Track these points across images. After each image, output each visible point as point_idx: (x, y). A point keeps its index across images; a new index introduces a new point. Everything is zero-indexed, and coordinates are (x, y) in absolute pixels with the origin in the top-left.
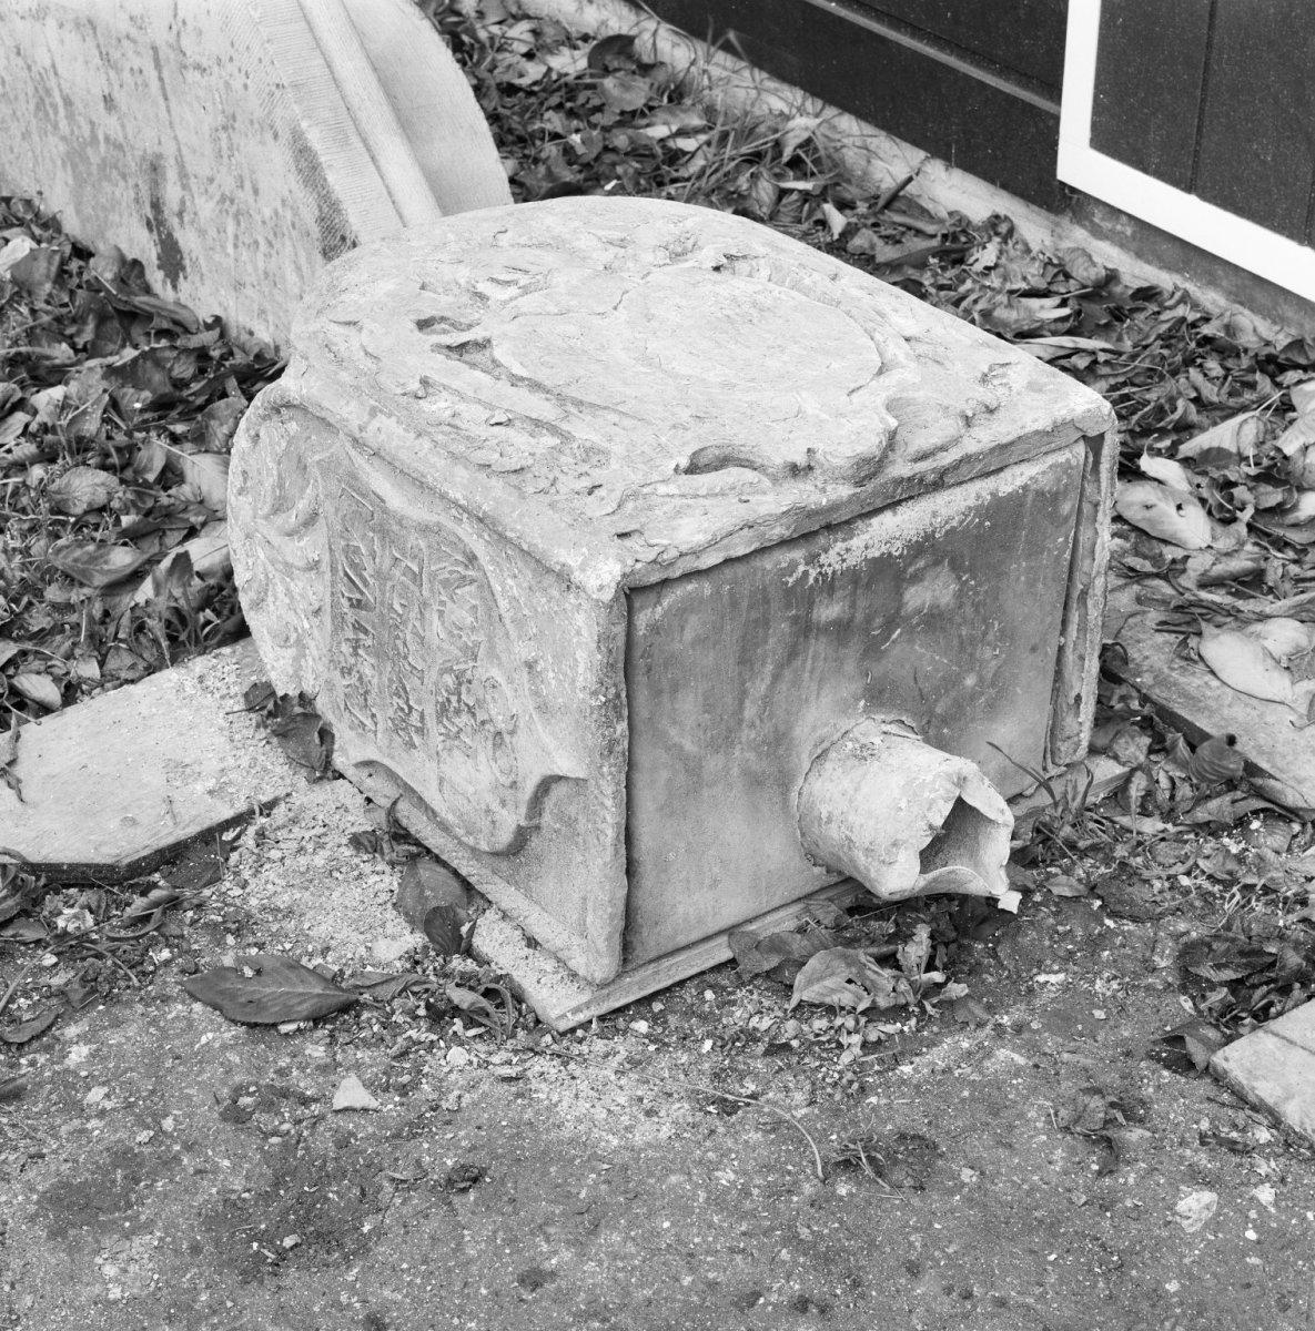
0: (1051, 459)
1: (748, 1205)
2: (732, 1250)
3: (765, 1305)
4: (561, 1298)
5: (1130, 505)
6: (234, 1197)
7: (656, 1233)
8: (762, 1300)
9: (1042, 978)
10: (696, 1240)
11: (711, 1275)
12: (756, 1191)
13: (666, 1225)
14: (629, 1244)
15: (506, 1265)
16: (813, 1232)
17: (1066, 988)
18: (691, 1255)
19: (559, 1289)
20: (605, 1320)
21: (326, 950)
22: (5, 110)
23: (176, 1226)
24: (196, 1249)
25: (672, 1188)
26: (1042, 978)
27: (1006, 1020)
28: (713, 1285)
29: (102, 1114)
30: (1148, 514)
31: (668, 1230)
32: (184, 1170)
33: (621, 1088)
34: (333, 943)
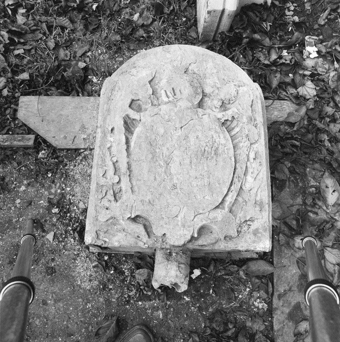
0: (47, 31)
1: (87, 315)
2: (76, 323)
3: (72, 338)
4: (45, 310)
5: (324, 182)
6: (19, 244)
7: (68, 309)
8: (72, 337)
9: (185, 297)
10: (73, 316)
11: (69, 325)
12: (91, 313)
13: (71, 309)
14: (63, 308)
15: (43, 295)
16: (92, 329)
17: (187, 302)
18: (70, 318)
19: (46, 308)
20: (47, 321)
21: (73, 196)
22: (339, 255)
23: (7, 244)
24: (7, 250)
25: (78, 302)
26: (185, 297)
27: (168, 303)
28: (68, 327)
29: (16, 207)
30: (325, 189)
31: (70, 310)
32: (16, 232)
33: (91, 270)
34: (76, 195)
